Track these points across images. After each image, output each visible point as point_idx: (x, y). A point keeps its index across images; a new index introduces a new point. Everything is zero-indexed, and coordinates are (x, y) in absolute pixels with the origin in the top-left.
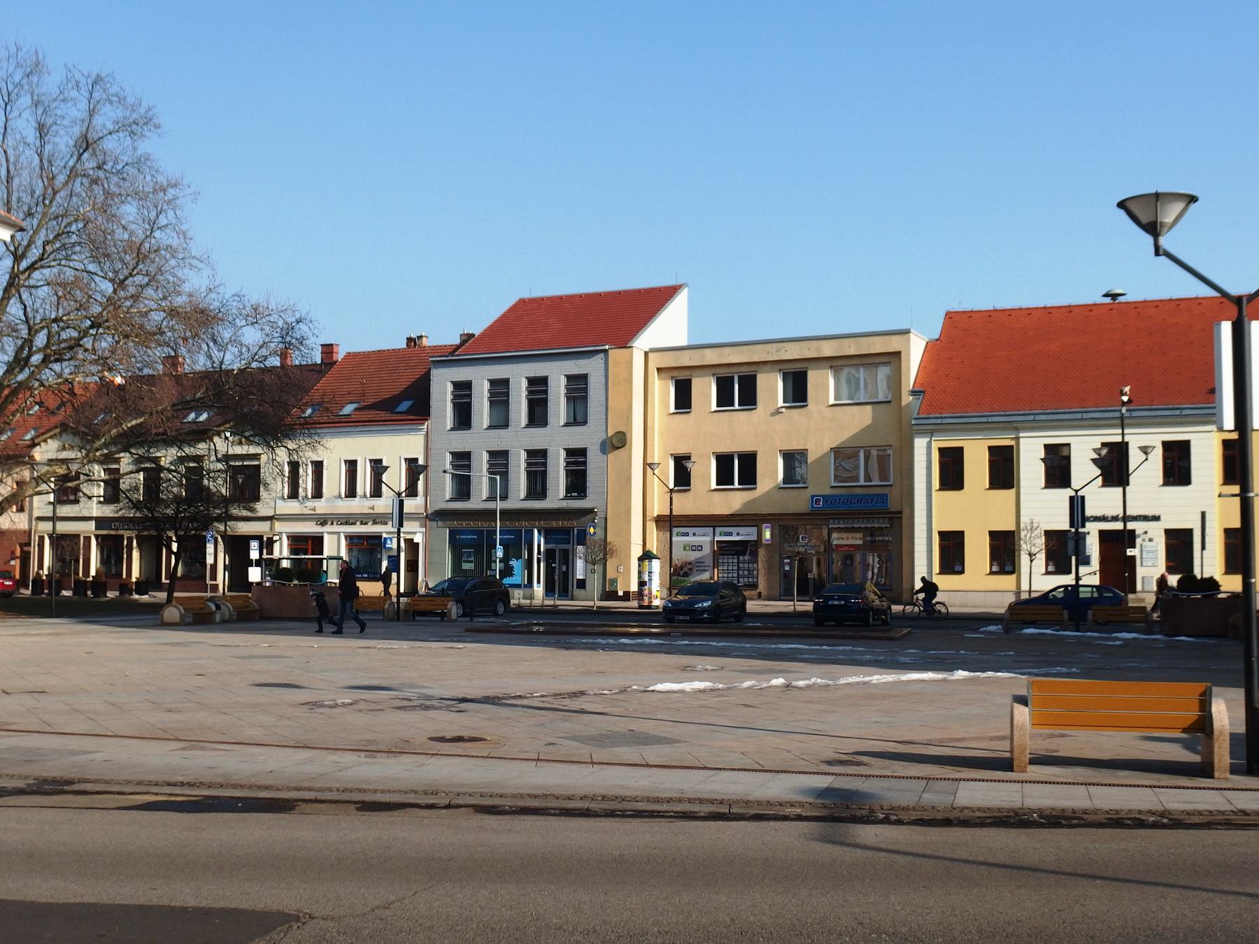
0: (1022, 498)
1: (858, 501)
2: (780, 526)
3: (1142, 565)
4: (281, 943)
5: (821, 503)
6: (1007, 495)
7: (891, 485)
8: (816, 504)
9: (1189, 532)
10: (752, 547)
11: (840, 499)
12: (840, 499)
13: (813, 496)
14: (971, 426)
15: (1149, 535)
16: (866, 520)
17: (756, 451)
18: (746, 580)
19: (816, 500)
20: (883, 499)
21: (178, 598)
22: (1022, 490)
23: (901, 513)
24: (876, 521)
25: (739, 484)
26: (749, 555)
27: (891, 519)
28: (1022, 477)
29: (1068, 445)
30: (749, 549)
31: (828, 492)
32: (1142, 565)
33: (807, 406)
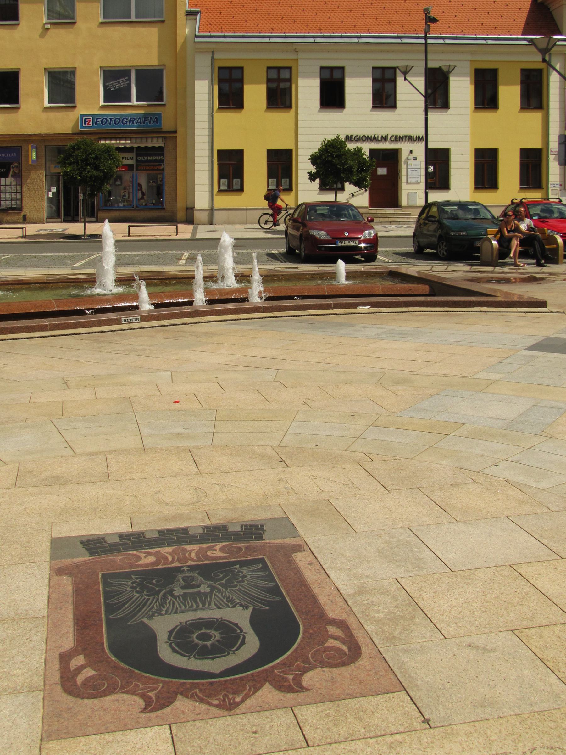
0: (300, 117)
1: (130, 121)
2: (45, 146)
3: (407, 183)
4: (533, 753)
5: (91, 123)
6: (536, 117)
7: (164, 105)
8: (85, 124)
9: (290, 151)
10: (15, 169)
11: (111, 119)
12: (111, 119)
13: (82, 116)
14: (381, 48)
15: (414, 155)
16: (139, 140)
17: (20, 69)
18: (8, 203)
19: (85, 119)
20: (156, 118)
21: (382, 252)
22: (300, 111)
23: (175, 132)
24: (150, 140)
25: (137, 101)
26: (12, 176)
27: (165, 138)
28: (300, 96)
29: (242, 68)
30: (12, 170)
31: (97, 112)
32: (407, 183)
33: (18, 24)
